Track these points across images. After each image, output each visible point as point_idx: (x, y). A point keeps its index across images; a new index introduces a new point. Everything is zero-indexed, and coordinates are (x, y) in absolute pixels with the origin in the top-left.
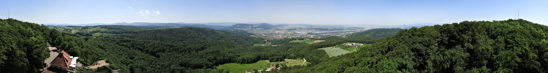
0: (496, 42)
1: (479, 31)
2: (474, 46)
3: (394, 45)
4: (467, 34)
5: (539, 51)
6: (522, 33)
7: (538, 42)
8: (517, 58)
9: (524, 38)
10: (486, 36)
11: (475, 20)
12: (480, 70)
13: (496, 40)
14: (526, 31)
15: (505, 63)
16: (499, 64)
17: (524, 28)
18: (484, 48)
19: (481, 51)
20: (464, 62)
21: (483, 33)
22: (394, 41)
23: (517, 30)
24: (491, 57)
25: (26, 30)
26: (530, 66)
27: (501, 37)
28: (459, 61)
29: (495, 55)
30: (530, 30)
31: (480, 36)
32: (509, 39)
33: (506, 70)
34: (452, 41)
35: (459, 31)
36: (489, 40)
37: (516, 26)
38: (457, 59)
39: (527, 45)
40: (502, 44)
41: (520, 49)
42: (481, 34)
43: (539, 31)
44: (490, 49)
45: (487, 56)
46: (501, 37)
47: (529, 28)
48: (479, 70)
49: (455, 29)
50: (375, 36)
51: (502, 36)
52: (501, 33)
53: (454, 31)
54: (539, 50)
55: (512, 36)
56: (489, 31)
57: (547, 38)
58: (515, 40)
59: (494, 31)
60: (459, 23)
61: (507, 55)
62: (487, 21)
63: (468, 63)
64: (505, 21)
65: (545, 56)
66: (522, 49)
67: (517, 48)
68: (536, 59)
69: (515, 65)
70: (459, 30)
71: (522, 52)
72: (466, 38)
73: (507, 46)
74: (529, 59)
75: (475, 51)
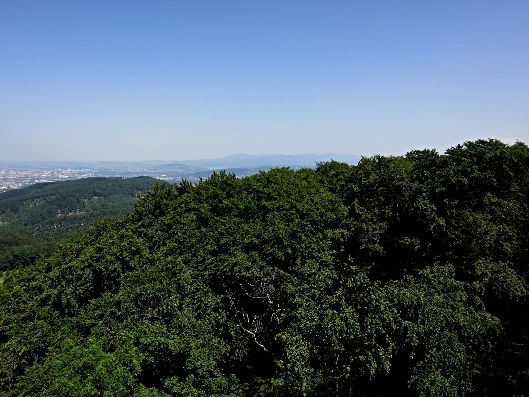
3: (123, 262)
22: (125, 243)
28: (438, 348)
34: (406, 240)
35: (444, 195)
38: (431, 332)
49: (421, 182)
50: (51, 223)
53: (419, 191)
60: (441, 152)
70: (444, 184)
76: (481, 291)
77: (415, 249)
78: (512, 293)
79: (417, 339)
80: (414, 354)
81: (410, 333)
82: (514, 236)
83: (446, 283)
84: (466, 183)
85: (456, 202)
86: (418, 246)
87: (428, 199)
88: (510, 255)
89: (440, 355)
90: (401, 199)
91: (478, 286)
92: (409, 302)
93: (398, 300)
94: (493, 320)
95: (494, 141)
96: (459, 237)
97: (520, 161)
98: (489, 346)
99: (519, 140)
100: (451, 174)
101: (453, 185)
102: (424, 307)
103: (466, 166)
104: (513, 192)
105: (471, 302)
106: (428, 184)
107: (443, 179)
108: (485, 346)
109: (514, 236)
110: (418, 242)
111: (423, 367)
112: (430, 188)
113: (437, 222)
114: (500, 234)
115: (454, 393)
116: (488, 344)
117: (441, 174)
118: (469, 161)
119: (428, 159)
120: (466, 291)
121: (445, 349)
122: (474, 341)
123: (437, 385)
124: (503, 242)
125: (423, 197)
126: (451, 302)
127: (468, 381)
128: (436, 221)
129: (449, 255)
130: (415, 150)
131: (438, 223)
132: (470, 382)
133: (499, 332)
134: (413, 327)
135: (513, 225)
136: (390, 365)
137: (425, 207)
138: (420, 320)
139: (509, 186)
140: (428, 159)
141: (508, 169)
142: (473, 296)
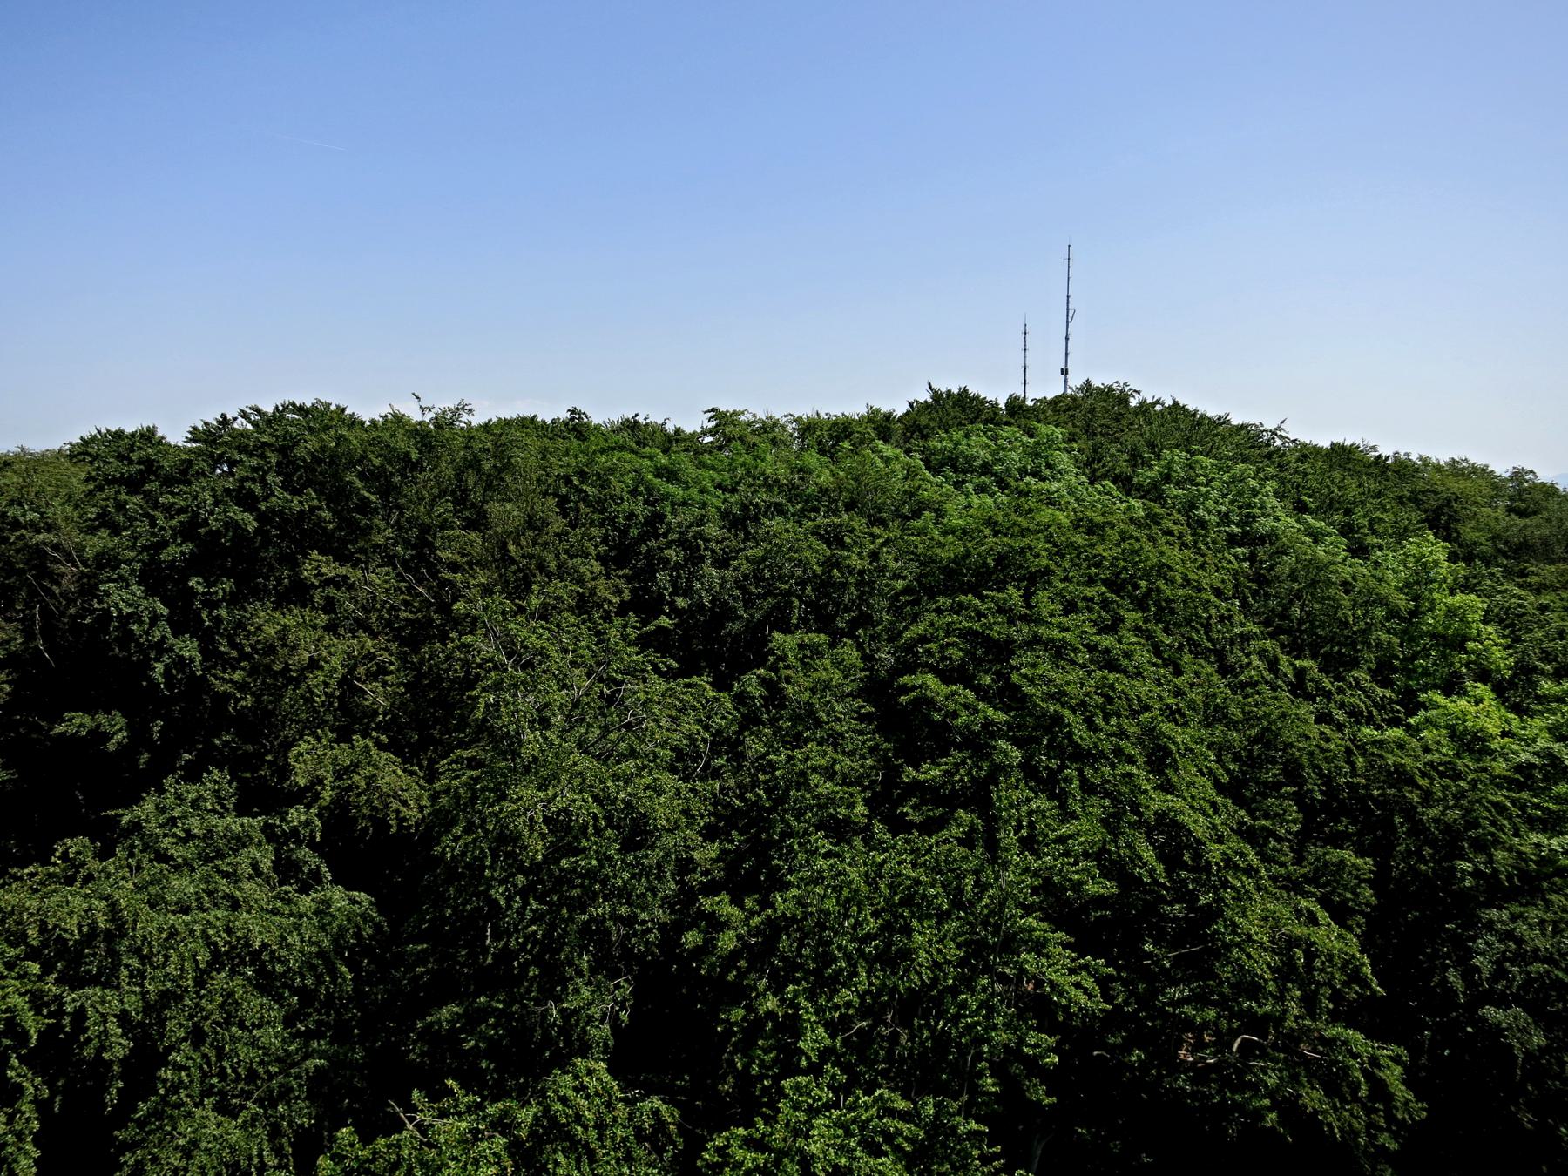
0: (749, 721)
1: (508, 560)
2: (432, 776)
4: (330, 605)
5: (1382, 870)
6: (1115, 585)
7: (1368, 732)
8: (1039, 947)
9: (1143, 657)
10: (613, 634)
11: (446, 403)
12: (526, 1115)
13: (752, 683)
14: (1174, 554)
15: (871, 1008)
16: (791, 1026)
17: (1154, 519)
18: (586, 809)
19: (536, 848)
20: (288, 1022)
21: (561, 589)
23: (1040, 545)
24: (679, 928)
25: (1350, 568)
26: (1243, 1086)
27: (816, 652)
28: (197, 1037)
29: (737, 901)
30: (1233, 540)
31: (531, 635)
32: (931, 680)
33: (891, 1113)
34: (77, 722)
35: (193, 565)
36: (659, 684)
37: (1025, 494)
38: (166, 997)
39: (1187, 772)
40: (835, 740)
41: (1086, 829)
42: (535, 601)
43: (1390, 558)
44: (662, 810)
45: (630, 921)
46: (816, 652)
47: (1225, 518)
48: (502, 1125)
49: (116, 530)
51: (836, 637)
52: (825, 585)
53: (106, 561)
54: (1380, 849)
55: (968, 635)
56: (655, 562)
57: (1525, 671)
58: (1011, 696)
59: (722, 563)
60: (176, 434)
61: (907, 901)
62: (631, 426)
63: (341, 1034)
64: (881, 425)
65: (1500, 973)
66: (1111, 824)
67: (1041, 803)
68: (1336, 997)
69: (1013, 1053)
70: (187, 532)
71: (1113, 868)
72: (314, 664)
73: (909, 774)
74: (1226, 973)
75: (449, 847)
76: (312, 831)
77: (111, 746)
78: (394, 815)
79: (122, 1036)
80: (121, 1084)
81: (95, 1024)
82: (391, 663)
83: (209, 834)
84: (250, 528)
85: (228, 585)
86: (120, 736)
87: (139, 583)
88: (385, 714)
89: (205, 1056)
90: (48, 591)
91: (303, 818)
92: (80, 926)
93: (43, 928)
94: (353, 901)
95: (333, 408)
96: (242, 687)
97: (390, 463)
98: (345, 979)
99: (396, 407)
100: (205, 501)
101: (216, 534)
102: (134, 929)
103: (247, 479)
104: (379, 546)
105: (286, 869)
106: (134, 538)
107: (182, 517)
108: (333, 981)
109: (391, 663)
110: (120, 721)
111: (157, 1113)
112: (145, 548)
113: (173, 651)
114: (351, 665)
115: (261, 1150)
116: (342, 975)
117: (174, 503)
118: (255, 461)
119: (135, 456)
120: (269, 842)
121: (217, 1033)
122: (303, 977)
123: (207, 1149)
124: (364, 683)
125: (121, 578)
126: (224, 886)
127: (298, 1098)
128: (171, 649)
129: (226, 744)
130: (108, 431)
131: (178, 655)
132: (303, 1101)
133: (370, 931)
134: (103, 1002)
135: (387, 634)
136: (37, 1154)
137: (130, 610)
138: (124, 972)
139: (366, 531)
140: (135, 456)
141: (359, 485)
142: (292, 850)
